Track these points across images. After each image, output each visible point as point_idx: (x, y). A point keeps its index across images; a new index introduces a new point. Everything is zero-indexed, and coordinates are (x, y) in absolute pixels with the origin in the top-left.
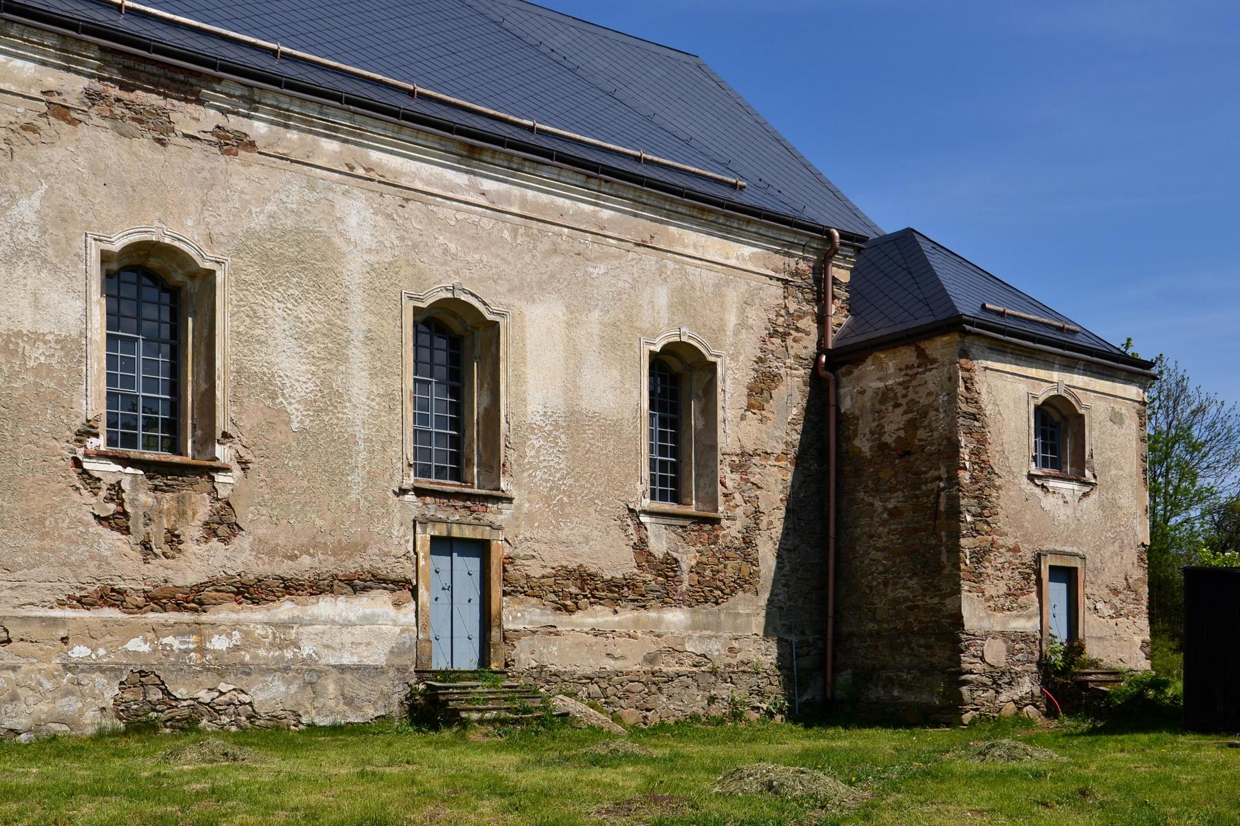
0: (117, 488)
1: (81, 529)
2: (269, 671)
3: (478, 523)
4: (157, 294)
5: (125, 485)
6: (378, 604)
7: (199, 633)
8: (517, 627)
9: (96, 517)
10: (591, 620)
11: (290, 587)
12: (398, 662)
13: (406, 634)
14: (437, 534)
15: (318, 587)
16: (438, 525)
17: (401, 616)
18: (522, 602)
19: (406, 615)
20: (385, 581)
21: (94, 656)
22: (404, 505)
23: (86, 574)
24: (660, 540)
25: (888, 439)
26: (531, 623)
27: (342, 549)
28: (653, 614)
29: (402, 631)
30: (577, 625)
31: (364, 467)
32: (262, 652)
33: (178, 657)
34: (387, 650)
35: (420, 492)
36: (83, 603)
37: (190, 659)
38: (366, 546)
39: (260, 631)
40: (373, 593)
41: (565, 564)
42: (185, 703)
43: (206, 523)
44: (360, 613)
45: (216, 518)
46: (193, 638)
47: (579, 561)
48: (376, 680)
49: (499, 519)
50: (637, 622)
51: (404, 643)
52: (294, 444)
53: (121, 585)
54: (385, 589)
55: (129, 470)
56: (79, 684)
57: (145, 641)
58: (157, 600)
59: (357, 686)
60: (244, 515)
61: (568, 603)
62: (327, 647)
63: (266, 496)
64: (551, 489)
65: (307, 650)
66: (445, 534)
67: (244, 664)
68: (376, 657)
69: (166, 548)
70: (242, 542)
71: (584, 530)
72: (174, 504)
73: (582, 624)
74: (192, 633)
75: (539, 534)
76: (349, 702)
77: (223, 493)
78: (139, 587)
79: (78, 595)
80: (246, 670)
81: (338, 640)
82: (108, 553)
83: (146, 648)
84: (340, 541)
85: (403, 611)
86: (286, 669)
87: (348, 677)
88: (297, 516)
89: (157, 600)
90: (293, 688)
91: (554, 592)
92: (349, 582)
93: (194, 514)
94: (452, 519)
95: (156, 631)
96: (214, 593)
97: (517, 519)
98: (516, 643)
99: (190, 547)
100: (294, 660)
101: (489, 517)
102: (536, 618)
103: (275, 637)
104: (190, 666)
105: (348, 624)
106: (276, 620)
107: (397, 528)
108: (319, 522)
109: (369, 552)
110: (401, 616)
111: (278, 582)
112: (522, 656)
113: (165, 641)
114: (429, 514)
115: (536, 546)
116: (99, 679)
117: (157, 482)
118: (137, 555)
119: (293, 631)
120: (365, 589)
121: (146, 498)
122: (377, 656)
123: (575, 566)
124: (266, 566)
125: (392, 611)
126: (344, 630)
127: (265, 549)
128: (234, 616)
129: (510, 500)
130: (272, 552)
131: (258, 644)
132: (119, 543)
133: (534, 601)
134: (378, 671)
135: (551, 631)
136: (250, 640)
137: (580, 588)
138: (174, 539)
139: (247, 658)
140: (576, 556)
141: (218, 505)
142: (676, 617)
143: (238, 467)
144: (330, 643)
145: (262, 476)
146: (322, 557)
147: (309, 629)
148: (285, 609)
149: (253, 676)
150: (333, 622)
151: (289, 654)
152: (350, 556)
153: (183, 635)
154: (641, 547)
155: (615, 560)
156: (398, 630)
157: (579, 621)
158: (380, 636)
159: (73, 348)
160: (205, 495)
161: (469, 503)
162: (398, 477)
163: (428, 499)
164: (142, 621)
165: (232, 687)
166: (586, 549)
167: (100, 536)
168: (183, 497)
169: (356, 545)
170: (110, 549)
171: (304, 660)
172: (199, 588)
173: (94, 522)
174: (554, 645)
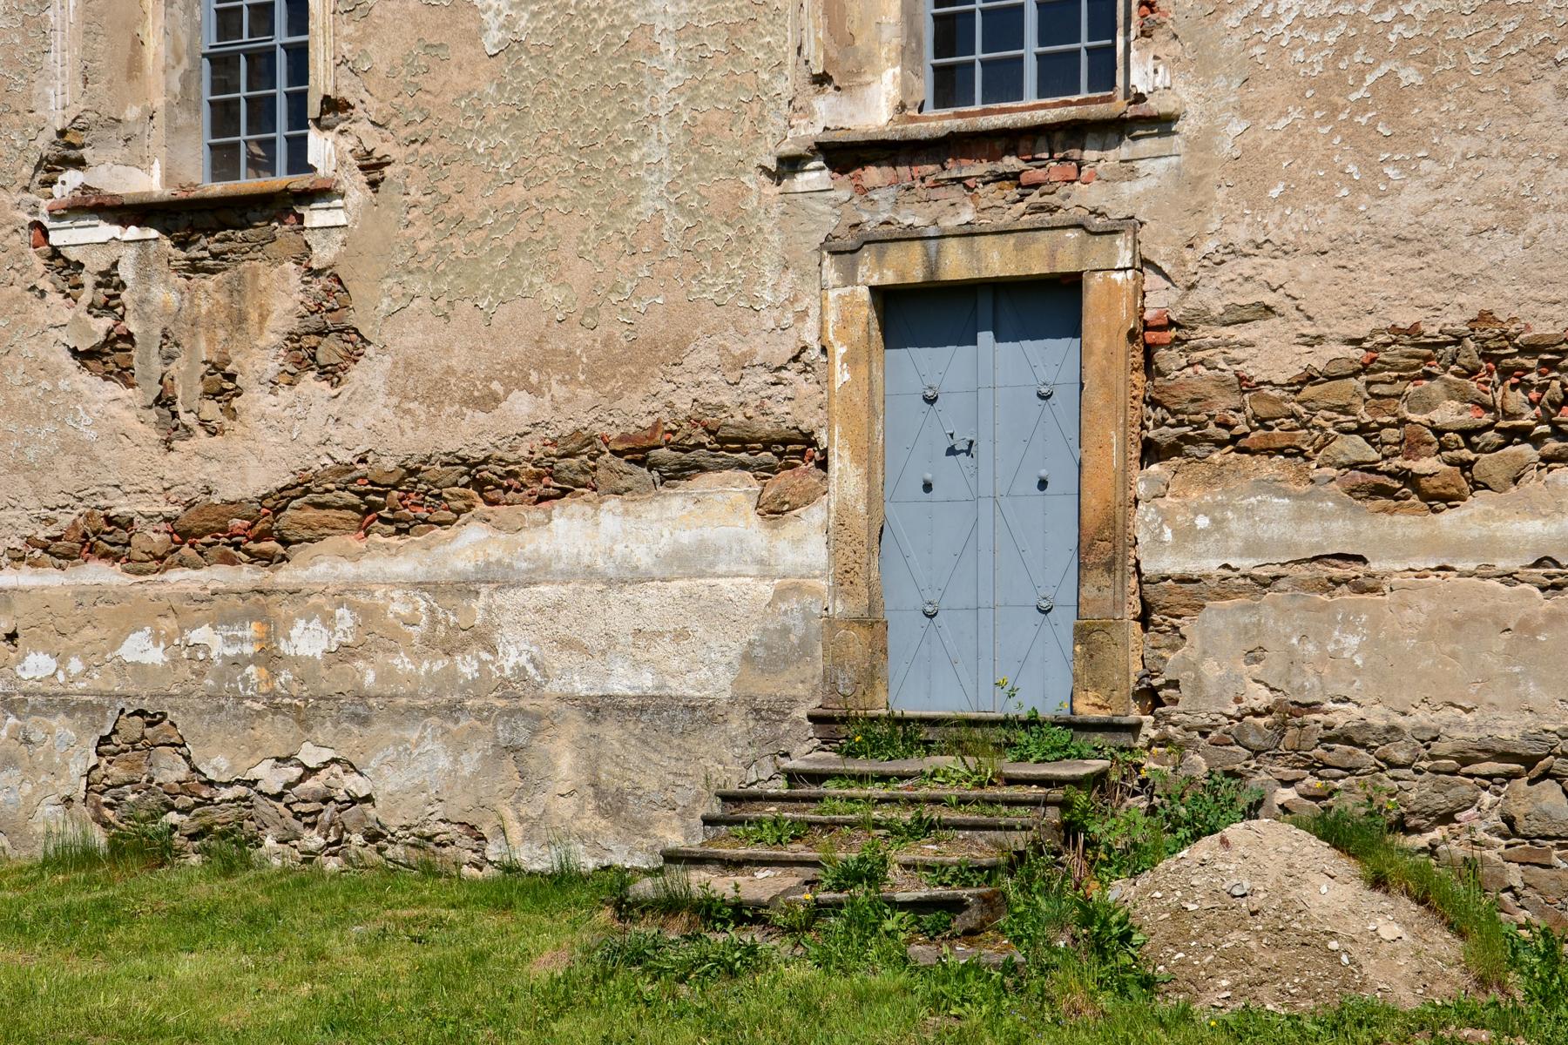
0: (109, 279)
1: (45, 384)
2: (412, 714)
3: (1046, 220)
5: (126, 272)
6: (721, 508)
7: (262, 616)
8: (1192, 567)
9: (75, 352)
10: (1533, 528)
11: (486, 482)
12: (767, 688)
13: (793, 604)
14: (890, 278)
15: (559, 475)
16: (894, 252)
17: (782, 546)
18: (1219, 474)
19: (797, 543)
20: (743, 443)
21: (61, 677)
22: (792, 206)
23: (56, 487)
26: (1252, 547)
27: (616, 362)
29: (780, 595)
30: (1462, 548)
31: (674, 115)
32: (402, 663)
33: (220, 676)
34: (737, 649)
37: (246, 680)
38: (680, 346)
39: (399, 608)
40: (702, 482)
41: (1404, 319)
42: (228, 794)
43: (293, 337)
44: (665, 545)
45: (314, 321)
46: (252, 630)
47: (1474, 301)
48: (691, 742)
49: (1124, 197)
51: (785, 631)
52: (491, 90)
53: (121, 507)
54: (743, 466)
55: (133, 232)
56: (27, 741)
57: (156, 638)
58: (203, 532)
59: (634, 759)
60: (370, 306)
61: (1426, 464)
62: (567, 644)
63: (424, 246)
64: (1345, 47)
65: (512, 657)
66: (917, 275)
67: (362, 697)
68: (704, 674)
69: (211, 409)
70: (369, 374)
71: (1502, 177)
72: (222, 298)
73: (1491, 545)
74: (251, 616)
75: (1289, 224)
76: (612, 804)
77: (322, 255)
78: (155, 510)
79: (41, 536)
80: (359, 711)
81: (597, 626)
82: (91, 434)
83: (156, 656)
84: (608, 342)
85: (791, 528)
86: (453, 710)
87: (611, 732)
88: (497, 284)
89: (203, 532)
90: (470, 763)
91: (1362, 430)
92: (638, 453)
93: (263, 318)
94: (949, 223)
95: (187, 609)
96: (311, 513)
97: (1195, 183)
98: (1185, 625)
99: (256, 401)
100: (477, 686)
101: (1087, 195)
102: (1275, 531)
103: (434, 622)
104: (240, 700)
105: (630, 577)
106: (444, 574)
107: (770, 277)
108: (552, 295)
109: (692, 362)
110: (782, 546)
111: (452, 474)
112: (1212, 670)
113: (196, 636)
114: (871, 220)
115: (1277, 271)
116: (61, 726)
117: (194, 252)
118: (148, 432)
119: (478, 605)
120: (683, 472)
121: (165, 293)
122: (707, 674)
123: (1455, 320)
124: (422, 432)
125: (751, 529)
126: (613, 596)
127: (425, 388)
128: (348, 569)
129: (1163, 124)
130: (436, 394)
131: (393, 640)
132: (115, 409)
133: (1270, 467)
134: (700, 714)
135: (1343, 572)
136: (374, 633)
138: (222, 385)
139: (370, 678)
140: (1462, 282)
141: (317, 286)
143: (361, 177)
144: (574, 633)
145: (415, 194)
146: (559, 391)
147: (521, 596)
148: (469, 544)
149: (377, 727)
150: (590, 574)
151: (467, 668)
152: (636, 379)
153: (229, 621)
156: (766, 589)
157: (1475, 531)
158: (716, 611)
160: (290, 266)
161: (1011, 163)
162: (775, 123)
163: (873, 175)
164: (152, 591)
165: (327, 755)
166: (1510, 248)
167: (78, 395)
168: (241, 279)
169: (654, 346)
170: (95, 424)
171: (505, 683)
172: (278, 501)
173: (71, 364)
174: (1348, 626)
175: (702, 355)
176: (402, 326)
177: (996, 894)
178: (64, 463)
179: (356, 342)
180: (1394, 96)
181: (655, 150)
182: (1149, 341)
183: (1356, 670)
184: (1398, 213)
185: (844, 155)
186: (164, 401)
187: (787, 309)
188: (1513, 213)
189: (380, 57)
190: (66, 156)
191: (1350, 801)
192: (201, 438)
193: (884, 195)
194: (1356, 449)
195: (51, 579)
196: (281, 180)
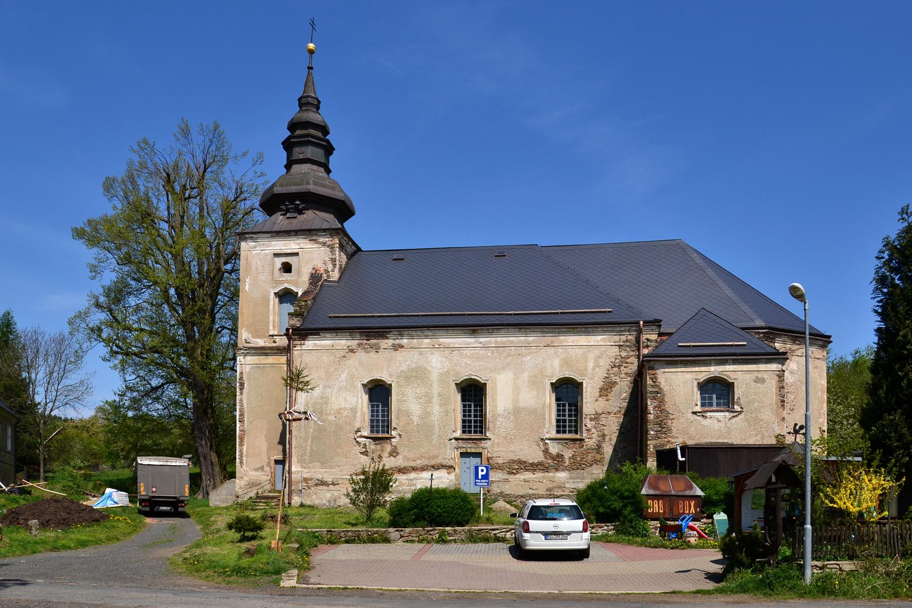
0: (365, 445)
4: (379, 392)
11: (414, 469)
28: (551, 474)
50: (544, 477)
60: (400, 450)
70: (400, 457)
75: (502, 449)
92: (433, 467)
101: (482, 445)
121: (373, 447)
125: (447, 475)
127: (406, 458)
131: (404, 485)
135: (506, 480)
137: (518, 466)
142: (562, 475)
148: (412, 475)
155: (536, 456)
175: (440, 457)
176: (403, 452)
177: (892, 270)
179: (398, 454)
180: (512, 439)
181: (435, 437)
182: (488, 459)
183: (507, 489)
184: (512, 449)
185: (456, 439)
186: (373, 459)
187: (451, 454)
188: (522, 450)
189: (401, 424)
190: (358, 431)
191: (507, 500)
193: (461, 443)
196: (386, 435)
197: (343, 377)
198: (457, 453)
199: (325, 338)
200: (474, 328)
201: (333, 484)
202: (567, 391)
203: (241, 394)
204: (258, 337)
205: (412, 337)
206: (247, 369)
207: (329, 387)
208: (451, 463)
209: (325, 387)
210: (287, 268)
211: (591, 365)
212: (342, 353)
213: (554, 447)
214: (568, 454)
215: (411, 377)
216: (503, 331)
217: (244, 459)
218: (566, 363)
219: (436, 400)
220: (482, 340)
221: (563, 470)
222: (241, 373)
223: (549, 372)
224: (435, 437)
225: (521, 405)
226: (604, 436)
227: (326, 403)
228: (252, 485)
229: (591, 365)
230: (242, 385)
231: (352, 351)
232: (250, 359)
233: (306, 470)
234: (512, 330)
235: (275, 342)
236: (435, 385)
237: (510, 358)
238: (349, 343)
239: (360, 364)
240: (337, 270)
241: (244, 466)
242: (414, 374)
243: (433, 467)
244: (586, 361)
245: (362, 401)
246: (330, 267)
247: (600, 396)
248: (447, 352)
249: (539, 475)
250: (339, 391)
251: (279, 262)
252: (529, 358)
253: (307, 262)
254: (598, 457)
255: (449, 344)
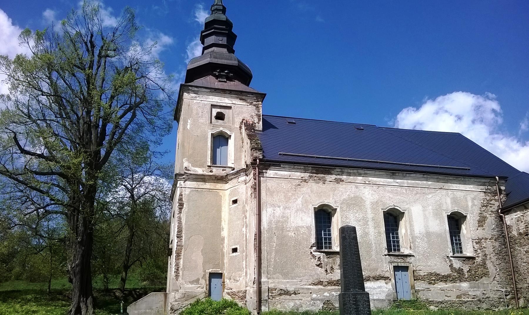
6: (382, 283)
12: (388, 298)
24: (457, 264)
25: (521, 231)
28: (458, 284)
35: (389, 255)
36: (314, 284)
49: (411, 261)
50: (453, 287)
83: (328, 295)
92: (374, 278)
120: (378, 280)
121: (326, 260)
137: (435, 278)
142: (465, 285)
154: (451, 266)
155: (445, 271)
156: (387, 290)
158: (383, 292)
159: (308, 228)
178: (316, 276)
185: (386, 255)
192: (330, 274)
194: (428, 281)
195: (315, 287)
197: (299, 201)
198: (392, 267)
199: (284, 169)
200: (394, 171)
201: (295, 293)
202: (456, 221)
203: (180, 212)
204: (197, 166)
205: (349, 174)
206: (187, 192)
207: (289, 208)
208: (387, 275)
209: (285, 208)
210: (220, 117)
211: (470, 204)
212: (297, 182)
213: (457, 263)
214: (466, 268)
215: (351, 204)
216: (412, 175)
217: (181, 272)
218: (455, 201)
219: (371, 223)
220: (398, 181)
221: (465, 281)
222: (181, 195)
223: (444, 207)
224: (373, 253)
225: (431, 230)
226: (485, 255)
227: (286, 221)
228: (186, 296)
229: (470, 204)
230: (181, 205)
231: (305, 181)
232: (189, 184)
233: (270, 281)
234: (418, 175)
235: (211, 171)
236: (369, 211)
237: (418, 195)
238: (303, 175)
239: (312, 192)
240: (261, 123)
241: (180, 278)
242: (353, 202)
243: (374, 278)
244: (467, 201)
245: (310, 220)
246: (256, 120)
247: (479, 226)
248: (375, 187)
249: (449, 285)
250: (296, 212)
251: (215, 111)
252: (430, 196)
253: (238, 114)
254: (485, 271)
255: (376, 181)
